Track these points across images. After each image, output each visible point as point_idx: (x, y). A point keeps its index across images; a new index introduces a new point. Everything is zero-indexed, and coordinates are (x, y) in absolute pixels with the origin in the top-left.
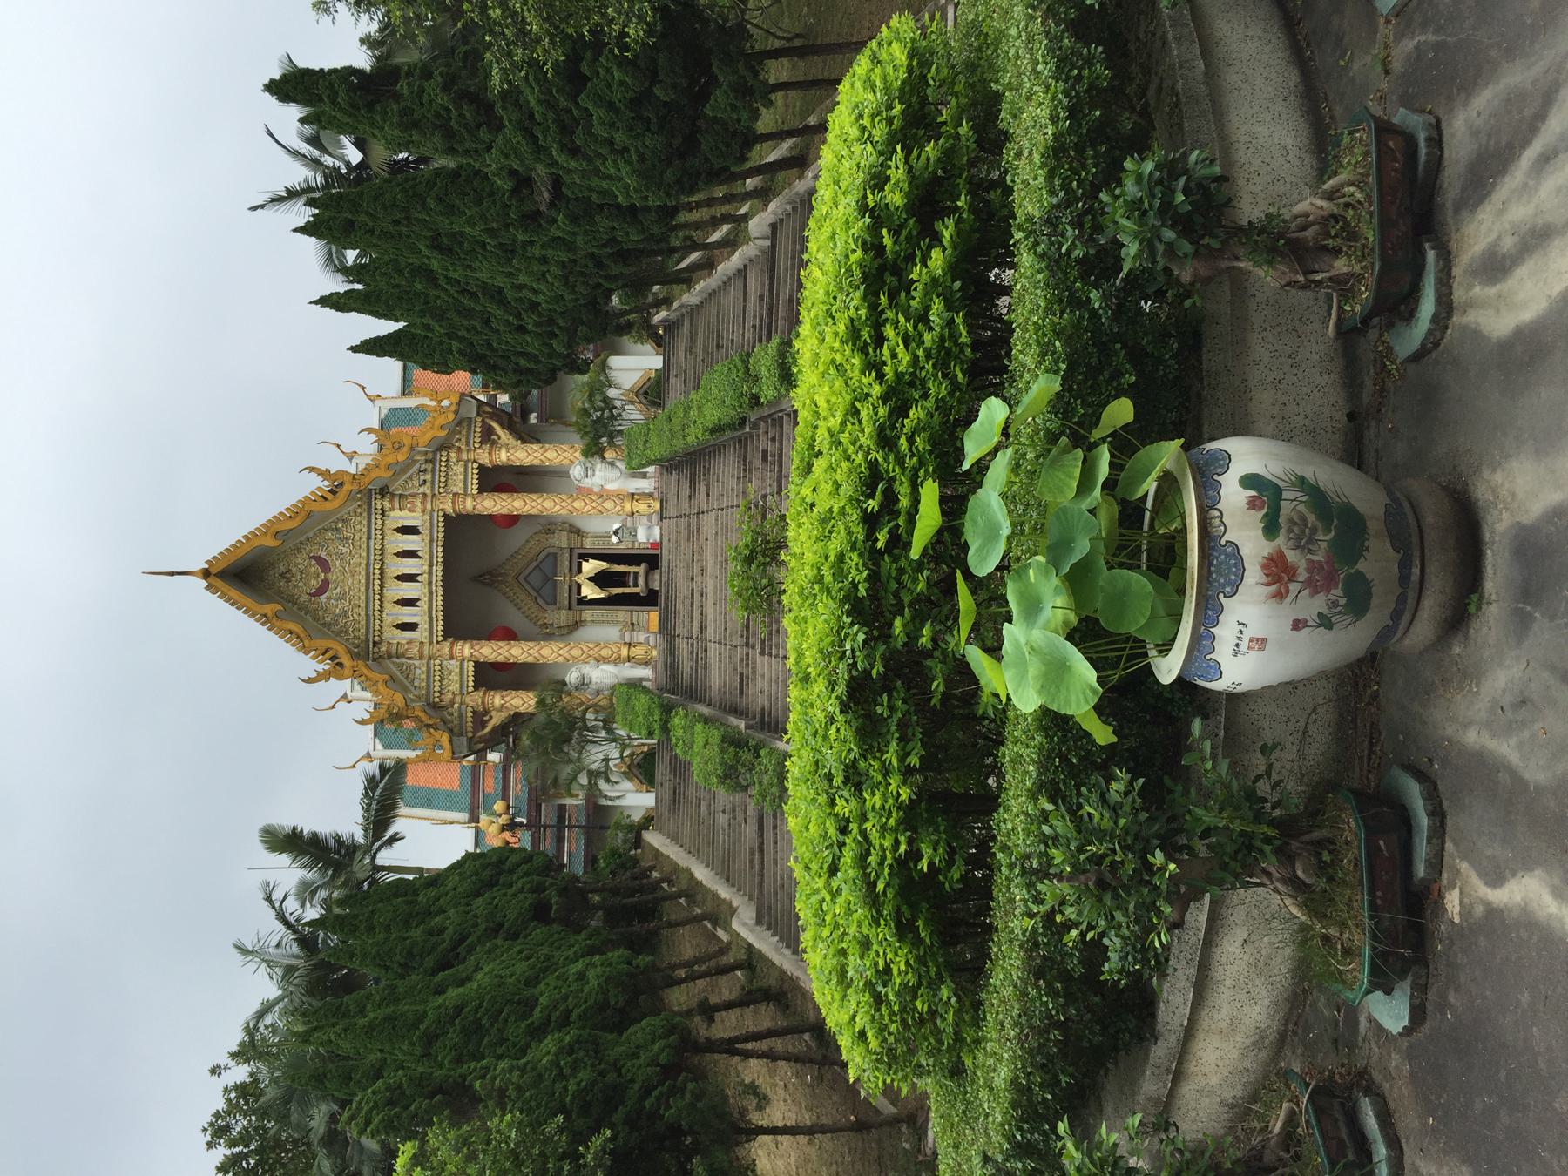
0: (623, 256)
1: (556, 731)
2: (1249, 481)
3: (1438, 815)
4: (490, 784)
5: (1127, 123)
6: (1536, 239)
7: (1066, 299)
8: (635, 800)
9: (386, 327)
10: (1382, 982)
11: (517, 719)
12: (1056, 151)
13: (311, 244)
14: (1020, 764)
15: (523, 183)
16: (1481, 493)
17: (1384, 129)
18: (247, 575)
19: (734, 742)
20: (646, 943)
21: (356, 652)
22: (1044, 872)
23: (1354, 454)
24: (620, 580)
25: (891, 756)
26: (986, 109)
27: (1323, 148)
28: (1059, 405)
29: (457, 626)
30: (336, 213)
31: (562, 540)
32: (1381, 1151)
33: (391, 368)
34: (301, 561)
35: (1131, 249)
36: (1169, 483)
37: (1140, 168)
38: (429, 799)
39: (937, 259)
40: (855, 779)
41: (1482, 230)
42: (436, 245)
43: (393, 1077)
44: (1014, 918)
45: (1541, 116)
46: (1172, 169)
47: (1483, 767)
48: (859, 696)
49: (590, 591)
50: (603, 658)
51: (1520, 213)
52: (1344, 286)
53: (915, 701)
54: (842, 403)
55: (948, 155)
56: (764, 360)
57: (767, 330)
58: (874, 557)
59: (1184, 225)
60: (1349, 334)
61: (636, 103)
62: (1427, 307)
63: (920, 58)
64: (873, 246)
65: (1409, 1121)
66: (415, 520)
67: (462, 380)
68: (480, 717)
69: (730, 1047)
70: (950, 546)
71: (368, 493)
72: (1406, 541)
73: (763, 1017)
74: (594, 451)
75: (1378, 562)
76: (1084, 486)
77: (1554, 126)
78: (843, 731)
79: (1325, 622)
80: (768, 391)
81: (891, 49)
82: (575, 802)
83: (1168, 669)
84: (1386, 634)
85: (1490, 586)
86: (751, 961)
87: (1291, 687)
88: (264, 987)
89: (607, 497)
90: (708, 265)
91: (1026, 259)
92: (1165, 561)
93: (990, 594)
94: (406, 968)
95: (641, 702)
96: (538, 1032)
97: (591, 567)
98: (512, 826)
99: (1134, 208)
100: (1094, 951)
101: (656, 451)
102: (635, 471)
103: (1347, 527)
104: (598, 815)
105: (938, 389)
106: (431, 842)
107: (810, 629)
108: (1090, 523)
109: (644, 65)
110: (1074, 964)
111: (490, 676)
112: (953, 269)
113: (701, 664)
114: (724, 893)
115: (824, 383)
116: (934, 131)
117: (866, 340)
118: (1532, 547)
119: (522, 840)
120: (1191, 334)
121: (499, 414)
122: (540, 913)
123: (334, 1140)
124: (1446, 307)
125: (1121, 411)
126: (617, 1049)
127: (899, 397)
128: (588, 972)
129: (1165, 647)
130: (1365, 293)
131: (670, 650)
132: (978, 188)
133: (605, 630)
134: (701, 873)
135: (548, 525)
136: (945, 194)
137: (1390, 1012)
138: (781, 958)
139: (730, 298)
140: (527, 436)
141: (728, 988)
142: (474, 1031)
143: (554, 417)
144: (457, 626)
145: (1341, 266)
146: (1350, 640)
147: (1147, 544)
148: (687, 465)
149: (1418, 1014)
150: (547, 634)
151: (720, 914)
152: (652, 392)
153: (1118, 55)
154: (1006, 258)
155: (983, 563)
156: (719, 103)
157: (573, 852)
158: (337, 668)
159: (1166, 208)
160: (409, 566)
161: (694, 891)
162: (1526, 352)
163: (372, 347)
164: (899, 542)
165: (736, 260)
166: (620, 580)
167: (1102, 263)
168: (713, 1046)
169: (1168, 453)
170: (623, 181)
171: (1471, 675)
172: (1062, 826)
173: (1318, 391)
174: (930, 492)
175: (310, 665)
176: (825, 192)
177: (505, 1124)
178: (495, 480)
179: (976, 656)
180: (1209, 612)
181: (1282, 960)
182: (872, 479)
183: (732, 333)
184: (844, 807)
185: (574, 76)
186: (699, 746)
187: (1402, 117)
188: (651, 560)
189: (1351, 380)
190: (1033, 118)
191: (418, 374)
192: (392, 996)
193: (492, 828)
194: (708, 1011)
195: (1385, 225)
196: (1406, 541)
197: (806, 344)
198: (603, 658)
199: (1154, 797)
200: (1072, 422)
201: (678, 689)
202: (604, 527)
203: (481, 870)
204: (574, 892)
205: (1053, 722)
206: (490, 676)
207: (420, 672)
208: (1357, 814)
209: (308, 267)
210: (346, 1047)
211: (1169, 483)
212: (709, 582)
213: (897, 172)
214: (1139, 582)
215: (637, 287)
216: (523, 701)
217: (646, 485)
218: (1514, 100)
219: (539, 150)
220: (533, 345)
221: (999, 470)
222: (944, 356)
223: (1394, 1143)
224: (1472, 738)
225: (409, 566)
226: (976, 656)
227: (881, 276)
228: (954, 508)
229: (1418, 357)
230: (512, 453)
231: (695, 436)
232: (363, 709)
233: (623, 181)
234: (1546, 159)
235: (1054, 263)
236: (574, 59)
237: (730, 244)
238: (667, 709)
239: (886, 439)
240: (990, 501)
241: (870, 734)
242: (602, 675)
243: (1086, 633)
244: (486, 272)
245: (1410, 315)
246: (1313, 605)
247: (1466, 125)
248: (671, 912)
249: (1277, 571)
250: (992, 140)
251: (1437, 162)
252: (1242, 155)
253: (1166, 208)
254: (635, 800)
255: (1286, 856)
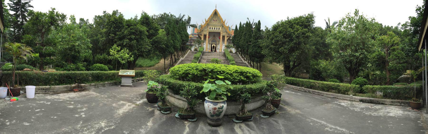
0: (244, 50)
1: (199, 42)
2: (223, 106)
3: (193, 122)
4: (195, 36)
5: (253, 94)
6: (243, 130)
7: (239, 89)
8: (193, 49)
9: (238, 28)
10: (179, 115)
11: (201, 38)
12: (251, 88)
13: (246, 22)
14: (199, 85)
15: (250, 42)
16: (221, 127)
17: (252, 116)
18: (216, 13)
19: (198, 58)
20: (180, 50)
21: (208, 23)
22: (189, 86)
23: (225, 115)
24: (214, 48)
25: (199, 73)
26: (255, 82)
27: (250, 111)
28: (230, 89)
29: (210, 33)
30: (248, 25)
31: (218, 43)
32: (166, 113)
33: (235, 28)
34: (217, 19)
35: (243, 95)
36: (223, 99)
37: (249, 96)
38: (193, 30)
39: (243, 78)
40: (197, 69)
41: (243, 125)
42: (245, 33)
43: (170, 28)
44: (185, 83)
45: (252, 130)
46: (249, 98)
47: (197, 126)
48: (204, 70)
49: (213, 45)
50: (206, 46)
51: (245, 129)
52: (239, 114)
53: (204, 75)
54: (231, 69)
55: (251, 79)
56: (234, 62)
57: (236, 62)
58: (217, 72)
59: (245, 100)
60: (235, 115)
61: (257, 52)
62: (237, 121)
63: (259, 77)
64: (244, 72)
65: (168, 116)
66: (220, 30)
67: (233, 35)
68: (201, 35)
69: (171, 57)
70: (218, 79)
71: (223, 26)
72: (217, 120)
73: (174, 60)
74: (226, 46)
75: (215, 118)
76: (223, 91)
77: (251, 131)
78: (201, 68)
79: (210, 113)
80: (231, 62)
81: (260, 74)
82: (193, 43)
83: (206, 98)
84: (209, 118)
85: (213, 128)
86: (178, 59)
87: (204, 109)
88: (177, 17)
89: (221, 47)
90: (242, 57)
91: (243, 86)
92: (216, 99)
93: (214, 82)
94: (178, 29)
95: (202, 50)
96: (173, 41)
97: (215, 45)
98: (191, 38)
99: (246, 95)
100: (182, 90)
101: (226, 52)
102: (224, 50)
103: (218, 115)
104: (191, 46)
105: (232, 78)
106: (190, 31)
107: (210, 66)
108: (220, 92)
109: (259, 53)
110: (181, 88)
111: (205, 36)
112: (242, 80)
113: (206, 55)
114: (184, 57)
115: (232, 68)
116: (253, 78)
117: (236, 72)
118: (216, 131)
119: (190, 39)
120: (235, 101)
121: (230, 38)
122: (183, 41)
123: (164, 23)
124: (237, 123)
125: (229, 94)
126: (172, 48)
127: (231, 75)
128: (178, 45)
129: (208, 98)
130: (238, 116)
131: (207, 53)
132: (249, 82)
133: (209, 47)
134: (186, 55)
135: (219, 42)
136: (249, 79)
137: (177, 115)
138: (178, 62)
139: (239, 59)
140: (227, 40)
141: (176, 57)
142: (173, 35)
143: (229, 43)
144: (210, 33)
145: (241, 113)
146: (208, 115)
147: (218, 97)
148: (224, 55)
149: (177, 118)
150: (209, 41)
151: (182, 56)
152: (231, 52)
153: (258, 93)
154: (242, 84)
155: (216, 82)
156: (256, 59)
157: (188, 43)
158: (206, 22)
159: (246, 98)
160: (216, 29)
161: (185, 54)
162: (233, 130)
163: (236, 27)
164: (218, 74)
165: (243, 60)
166: (214, 48)
167: (242, 93)
168: (172, 56)
169: (225, 99)
170: (250, 50)
171: (205, 125)
172: (193, 88)
173: (230, 112)
174: (223, 77)
175: (207, 19)
176: (249, 68)
177: (166, 38)
178: (224, 37)
179: (208, 81)
180: (212, 102)
181: (180, 106)
182: (224, 72)
183: (236, 59)
184: (194, 68)
185: (259, 47)
186: (198, 55)
187: (253, 118)
188: (215, 51)
189: (231, 115)
190: (254, 86)
191: (234, 31)
192: (176, 28)
193: (191, 36)
194: (174, 56)
195: (244, 117)
196: (217, 120)
197: (236, 66)
198: (206, 46)
199: (195, 96)
200: (229, 90)
201: (203, 53)
202: (218, 47)
203: (187, 35)
204: (184, 44)
205: (202, 88)
206: (205, 36)
207: (206, 29)
208: (193, 115)
209: (244, 22)
210: (172, 24)
211: (223, 99)
212: (213, 56)
213: (250, 75)
214: (214, 96)
215: (241, 51)
216: (202, 39)
217: (222, 51)
218: (253, 127)
219: (253, 43)
220: (236, 41)
221: (225, 84)
222: (234, 79)
223: (166, 114)
224: (200, 125)
225: (216, 29)
226: (208, 81)
227: (242, 73)
228: (221, 79)
229: (233, 121)
230: (226, 39)
231: (227, 56)
232: (202, 24)
233: (250, 50)
234: (249, 131)
235: (242, 89)
236: (261, 47)
237: (244, 59)
238: (201, 52)
239: (227, 73)
240: (222, 83)
241: (201, 71)
242: (205, 46)
243: (210, 91)
244: (243, 38)
245: (236, 120)
246: (212, 112)
247: (252, 123)
248: (183, 52)
249: (215, 109)
250: (252, 83)
251: (249, 121)
252: (250, 104)
253: (246, 98)
254: (193, 49)
255: (190, 108)
